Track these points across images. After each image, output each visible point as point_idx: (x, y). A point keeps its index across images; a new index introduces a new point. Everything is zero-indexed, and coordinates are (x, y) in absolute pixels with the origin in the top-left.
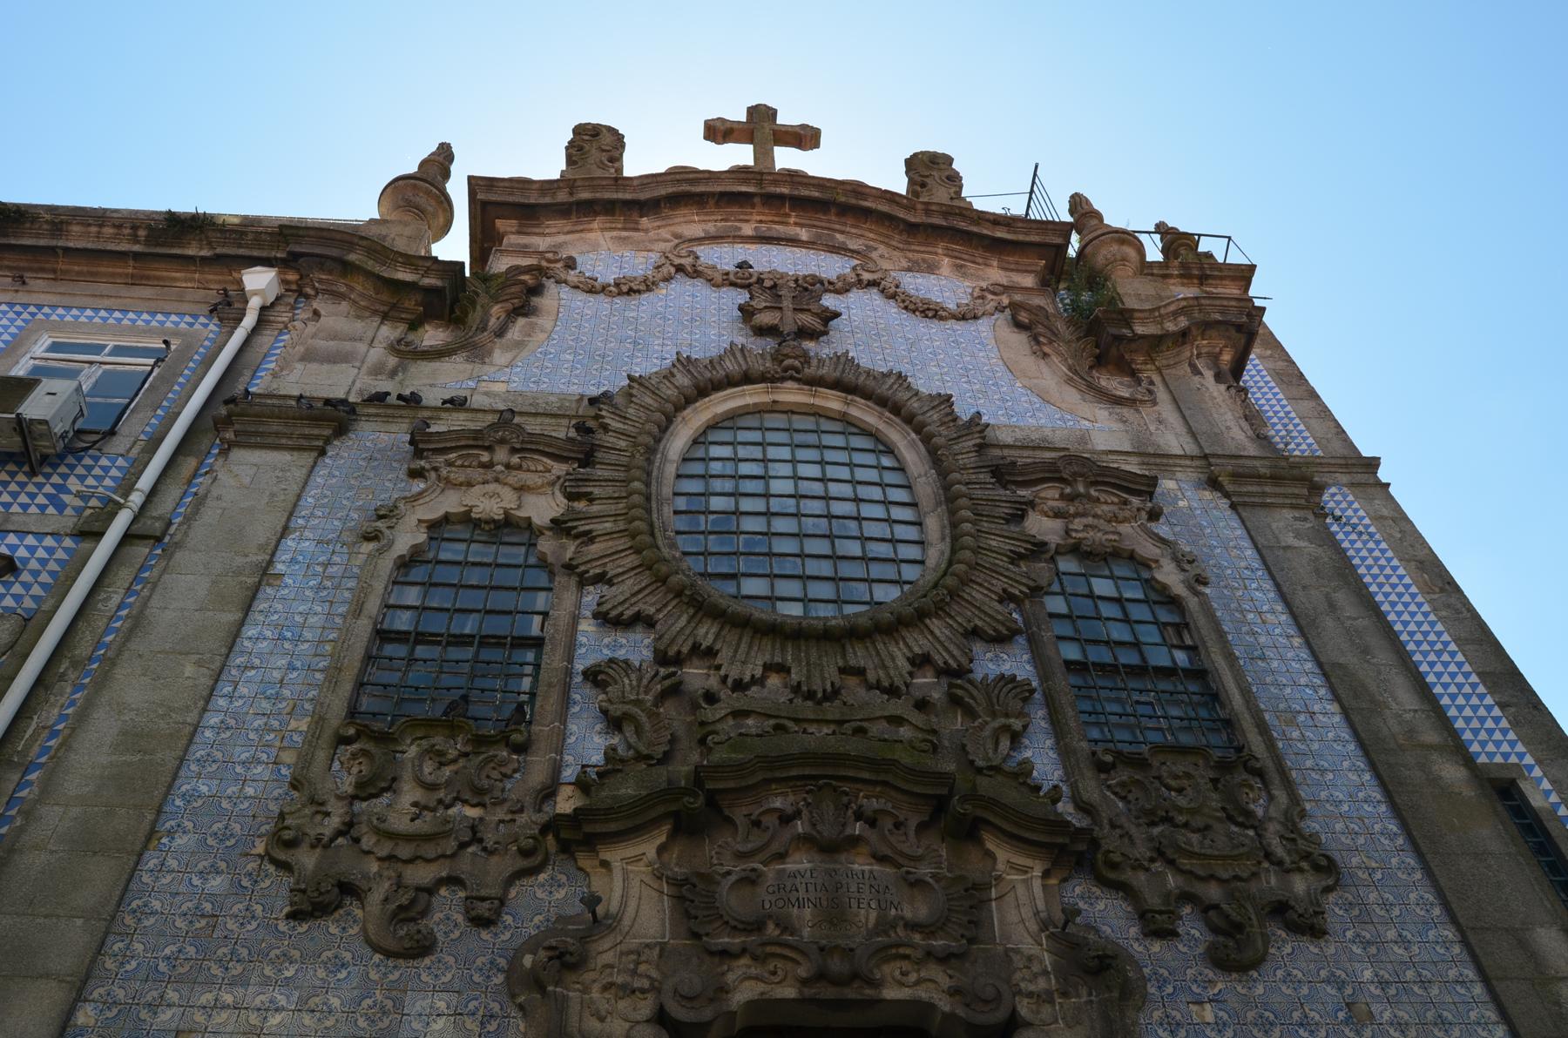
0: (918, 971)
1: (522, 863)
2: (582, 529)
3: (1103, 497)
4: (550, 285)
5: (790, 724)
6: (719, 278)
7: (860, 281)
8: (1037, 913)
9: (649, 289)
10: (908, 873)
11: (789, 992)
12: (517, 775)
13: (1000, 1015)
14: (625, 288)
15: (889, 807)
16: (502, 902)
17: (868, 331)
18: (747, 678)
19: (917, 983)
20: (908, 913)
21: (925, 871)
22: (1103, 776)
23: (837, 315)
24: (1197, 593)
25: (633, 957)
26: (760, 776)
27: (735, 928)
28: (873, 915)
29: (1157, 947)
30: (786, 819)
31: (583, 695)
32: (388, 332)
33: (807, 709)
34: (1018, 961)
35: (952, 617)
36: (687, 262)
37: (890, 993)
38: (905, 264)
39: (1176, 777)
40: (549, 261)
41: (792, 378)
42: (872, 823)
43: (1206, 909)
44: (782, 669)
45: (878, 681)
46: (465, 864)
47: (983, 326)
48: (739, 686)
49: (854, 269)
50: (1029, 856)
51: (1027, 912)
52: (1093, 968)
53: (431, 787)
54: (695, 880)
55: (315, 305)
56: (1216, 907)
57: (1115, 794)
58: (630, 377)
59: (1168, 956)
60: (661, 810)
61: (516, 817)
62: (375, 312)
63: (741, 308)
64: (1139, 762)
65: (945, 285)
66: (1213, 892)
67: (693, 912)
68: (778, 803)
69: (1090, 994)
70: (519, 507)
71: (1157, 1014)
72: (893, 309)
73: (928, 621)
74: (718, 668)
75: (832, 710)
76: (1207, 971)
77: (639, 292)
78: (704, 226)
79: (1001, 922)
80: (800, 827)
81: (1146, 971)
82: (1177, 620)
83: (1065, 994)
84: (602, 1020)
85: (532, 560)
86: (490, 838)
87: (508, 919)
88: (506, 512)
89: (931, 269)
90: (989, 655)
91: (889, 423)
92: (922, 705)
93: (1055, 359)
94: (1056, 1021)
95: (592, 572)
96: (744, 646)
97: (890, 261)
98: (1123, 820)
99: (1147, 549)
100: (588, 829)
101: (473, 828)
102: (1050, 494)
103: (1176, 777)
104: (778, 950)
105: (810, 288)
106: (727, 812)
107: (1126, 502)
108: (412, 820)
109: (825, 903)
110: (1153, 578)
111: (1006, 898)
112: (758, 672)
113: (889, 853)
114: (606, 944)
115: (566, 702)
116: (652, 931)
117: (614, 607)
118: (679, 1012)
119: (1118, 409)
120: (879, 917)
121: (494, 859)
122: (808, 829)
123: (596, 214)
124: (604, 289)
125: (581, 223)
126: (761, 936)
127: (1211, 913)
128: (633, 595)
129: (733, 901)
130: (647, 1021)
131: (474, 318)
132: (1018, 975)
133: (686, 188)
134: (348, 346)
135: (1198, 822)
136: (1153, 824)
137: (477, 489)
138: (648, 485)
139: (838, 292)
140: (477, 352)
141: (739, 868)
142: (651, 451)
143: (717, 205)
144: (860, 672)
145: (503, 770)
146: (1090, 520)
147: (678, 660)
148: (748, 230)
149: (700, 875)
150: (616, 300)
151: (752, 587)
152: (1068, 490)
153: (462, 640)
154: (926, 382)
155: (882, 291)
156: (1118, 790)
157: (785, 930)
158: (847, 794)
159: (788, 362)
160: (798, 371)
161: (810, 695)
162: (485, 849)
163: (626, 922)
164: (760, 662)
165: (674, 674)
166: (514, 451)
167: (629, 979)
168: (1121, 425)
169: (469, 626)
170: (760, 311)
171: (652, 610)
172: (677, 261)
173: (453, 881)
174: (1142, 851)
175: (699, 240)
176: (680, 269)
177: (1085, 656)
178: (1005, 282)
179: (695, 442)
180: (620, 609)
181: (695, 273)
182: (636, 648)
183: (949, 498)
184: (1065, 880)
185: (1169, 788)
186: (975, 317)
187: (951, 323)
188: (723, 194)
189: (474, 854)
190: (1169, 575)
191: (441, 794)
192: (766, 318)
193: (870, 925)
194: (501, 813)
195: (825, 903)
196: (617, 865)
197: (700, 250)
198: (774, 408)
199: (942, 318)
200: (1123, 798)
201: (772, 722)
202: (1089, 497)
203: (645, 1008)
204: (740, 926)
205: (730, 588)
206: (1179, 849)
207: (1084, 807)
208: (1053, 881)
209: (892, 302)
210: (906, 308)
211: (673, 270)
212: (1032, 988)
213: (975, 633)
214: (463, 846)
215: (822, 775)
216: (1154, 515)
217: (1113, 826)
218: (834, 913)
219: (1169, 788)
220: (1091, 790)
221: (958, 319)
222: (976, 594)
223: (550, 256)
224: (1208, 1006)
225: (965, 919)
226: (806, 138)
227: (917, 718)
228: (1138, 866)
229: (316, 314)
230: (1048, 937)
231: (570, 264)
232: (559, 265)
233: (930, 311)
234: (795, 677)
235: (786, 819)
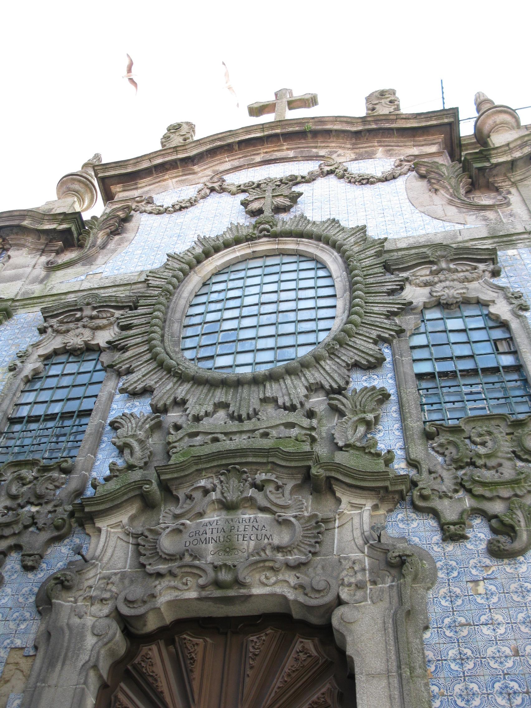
0: (276, 575)
1: (56, 534)
2: (123, 344)
3: (459, 268)
4: (136, 216)
5: (220, 436)
6: (234, 189)
7: (322, 172)
8: (363, 533)
9: (192, 205)
10: (280, 516)
11: (193, 595)
12: (64, 486)
13: (329, 598)
14: (177, 207)
15: (273, 478)
16: (41, 557)
17: (324, 202)
18: (202, 413)
19: (274, 584)
20: (276, 541)
21: (289, 515)
22: (430, 442)
23: (300, 194)
24: (519, 317)
25: (105, 581)
26: (195, 468)
27: (165, 559)
28: (252, 543)
29: (450, 547)
30: (206, 492)
31: (108, 437)
32: (44, 259)
33: (234, 426)
34: (347, 564)
35: (339, 358)
36: (216, 185)
37: (257, 591)
38: (353, 156)
39: (480, 435)
40: (138, 202)
41: (265, 236)
42: (260, 487)
43: (488, 517)
44: (225, 406)
45: (284, 403)
46: (24, 540)
47: (400, 182)
48: (197, 419)
49: (320, 166)
50: (362, 497)
51: (357, 533)
52: (397, 563)
53: (14, 497)
54: (147, 533)
55: (9, 253)
56: (496, 517)
57: (437, 452)
58: (168, 255)
59: (459, 552)
60: (132, 494)
61: (57, 508)
62: (38, 250)
63: (242, 204)
64: (455, 430)
65: (379, 164)
66: (497, 508)
67: (143, 552)
68: (202, 483)
69: (393, 581)
70: (93, 339)
71: (443, 591)
72: (342, 185)
73: (322, 363)
74: (186, 410)
75: (248, 425)
76: (484, 560)
77: (186, 207)
78: (232, 162)
79: (339, 541)
80: (214, 496)
81: (439, 564)
82: (507, 336)
83: (374, 583)
84: (80, 617)
85: (99, 367)
86: (40, 522)
87: (44, 566)
88: (86, 343)
89: (370, 156)
90: (364, 378)
91: (322, 250)
92: (311, 414)
93: (442, 192)
94: (366, 600)
95: (124, 367)
96: (202, 396)
97: (343, 156)
98: (439, 469)
99: (487, 295)
100: (87, 509)
101: (33, 517)
102: (423, 273)
103: (480, 435)
104: (189, 570)
105: (294, 180)
106: (175, 493)
107: (475, 268)
108: (3, 516)
109: (222, 539)
110: (490, 313)
111: (346, 526)
112: (210, 409)
113: (269, 505)
114: (91, 574)
115: (99, 441)
116: (120, 565)
117: (129, 386)
118: (125, 610)
119: (483, 213)
120: (256, 545)
121: (43, 533)
122: (219, 496)
123: (167, 170)
124: (166, 211)
125: (159, 177)
126: (183, 562)
127: (493, 521)
128: (143, 376)
129: (167, 544)
130: (107, 616)
131: (89, 242)
132: (345, 573)
133: (219, 143)
134: (20, 271)
135: (492, 462)
136: (462, 468)
137: (71, 333)
138: (165, 314)
139: (308, 182)
140: (87, 260)
141: (173, 525)
142: (169, 294)
143: (240, 149)
144: (275, 400)
145: (56, 484)
146: (448, 283)
147: (165, 410)
148: (258, 159)
149: (150, 531)
150: (173, 215)
151: (221, 361)
152: (435, 268)
153: (51, 417)
154: (349, 222)
155: (336, 175)
156: (438, 449)
157: (195, 558)
158: (246, 472)
159: (262, 226)
160: (268, 231)
161: (240, 419)
162: (38, 529)
163: (105, 560)
164: (212, 403)
165: (158, 417)
166: (94, 308)
167: (99, 593)
168: (483, 223)
169: (56, 408)
170: (252, 201)
171: (153, 382)
172: (210, 185)
173: (18, 547)
174: (448, 485)
175: (227, 171)
176: (212, 190)
177: (435, 368)
178: (416, 153)
179: (204, 284)
180: (135, 385)
181: (223, 190)
182: (142, 408)
183: (352, 286)
184: (391, 511)
185: (474, 443)
186: (394, 178)
187: (380, 185)
188: (240, 143)
189: (32, 532)
190: (502, 309)
191: (19, 501)
192: (255, 206)
193: (250, 550)
194: (50, 507)
195: (222, 539)
196: (104, 529)
197: (226, 177)
198: (255, 256)
199: (372, 183)
200: (443, 454)
201: (210, 436)
202: (449, 270)
203: (106, 610)
204: (168, 557)
205: (209, 364)
206: (474, 482)
207: (413, 464)
208: (382, 512)
209: (342, 180)
210: (350, 182)
211: (208, 191)
212: (353, 580)
213: (356, 365)
214: (26, 527)
215: (229, 464)
216: (496, 273)
217: (430, 472)
218: (228, 546)
219: (474, 443)
220: (419, 451)
221: (383, 181)
222: (359, 342)
223: (138, 199)
224: (481, 583)
225: (313, 541)
226: (311, 101)
227: (306, 422)
228: (443, 496)
229: (9, 257)
230: (369, 547)
231: (150, 201)
232: (143, 203)
233: (365, 181)
234: (231, 409)
235: (206, 492)
